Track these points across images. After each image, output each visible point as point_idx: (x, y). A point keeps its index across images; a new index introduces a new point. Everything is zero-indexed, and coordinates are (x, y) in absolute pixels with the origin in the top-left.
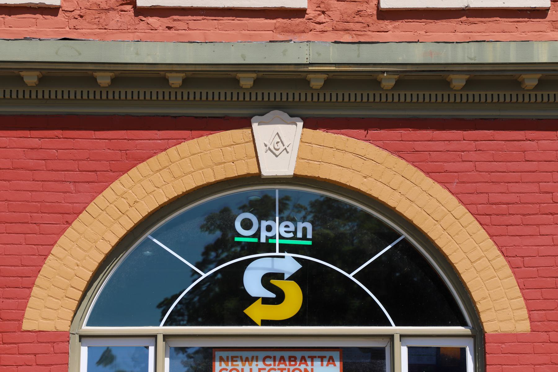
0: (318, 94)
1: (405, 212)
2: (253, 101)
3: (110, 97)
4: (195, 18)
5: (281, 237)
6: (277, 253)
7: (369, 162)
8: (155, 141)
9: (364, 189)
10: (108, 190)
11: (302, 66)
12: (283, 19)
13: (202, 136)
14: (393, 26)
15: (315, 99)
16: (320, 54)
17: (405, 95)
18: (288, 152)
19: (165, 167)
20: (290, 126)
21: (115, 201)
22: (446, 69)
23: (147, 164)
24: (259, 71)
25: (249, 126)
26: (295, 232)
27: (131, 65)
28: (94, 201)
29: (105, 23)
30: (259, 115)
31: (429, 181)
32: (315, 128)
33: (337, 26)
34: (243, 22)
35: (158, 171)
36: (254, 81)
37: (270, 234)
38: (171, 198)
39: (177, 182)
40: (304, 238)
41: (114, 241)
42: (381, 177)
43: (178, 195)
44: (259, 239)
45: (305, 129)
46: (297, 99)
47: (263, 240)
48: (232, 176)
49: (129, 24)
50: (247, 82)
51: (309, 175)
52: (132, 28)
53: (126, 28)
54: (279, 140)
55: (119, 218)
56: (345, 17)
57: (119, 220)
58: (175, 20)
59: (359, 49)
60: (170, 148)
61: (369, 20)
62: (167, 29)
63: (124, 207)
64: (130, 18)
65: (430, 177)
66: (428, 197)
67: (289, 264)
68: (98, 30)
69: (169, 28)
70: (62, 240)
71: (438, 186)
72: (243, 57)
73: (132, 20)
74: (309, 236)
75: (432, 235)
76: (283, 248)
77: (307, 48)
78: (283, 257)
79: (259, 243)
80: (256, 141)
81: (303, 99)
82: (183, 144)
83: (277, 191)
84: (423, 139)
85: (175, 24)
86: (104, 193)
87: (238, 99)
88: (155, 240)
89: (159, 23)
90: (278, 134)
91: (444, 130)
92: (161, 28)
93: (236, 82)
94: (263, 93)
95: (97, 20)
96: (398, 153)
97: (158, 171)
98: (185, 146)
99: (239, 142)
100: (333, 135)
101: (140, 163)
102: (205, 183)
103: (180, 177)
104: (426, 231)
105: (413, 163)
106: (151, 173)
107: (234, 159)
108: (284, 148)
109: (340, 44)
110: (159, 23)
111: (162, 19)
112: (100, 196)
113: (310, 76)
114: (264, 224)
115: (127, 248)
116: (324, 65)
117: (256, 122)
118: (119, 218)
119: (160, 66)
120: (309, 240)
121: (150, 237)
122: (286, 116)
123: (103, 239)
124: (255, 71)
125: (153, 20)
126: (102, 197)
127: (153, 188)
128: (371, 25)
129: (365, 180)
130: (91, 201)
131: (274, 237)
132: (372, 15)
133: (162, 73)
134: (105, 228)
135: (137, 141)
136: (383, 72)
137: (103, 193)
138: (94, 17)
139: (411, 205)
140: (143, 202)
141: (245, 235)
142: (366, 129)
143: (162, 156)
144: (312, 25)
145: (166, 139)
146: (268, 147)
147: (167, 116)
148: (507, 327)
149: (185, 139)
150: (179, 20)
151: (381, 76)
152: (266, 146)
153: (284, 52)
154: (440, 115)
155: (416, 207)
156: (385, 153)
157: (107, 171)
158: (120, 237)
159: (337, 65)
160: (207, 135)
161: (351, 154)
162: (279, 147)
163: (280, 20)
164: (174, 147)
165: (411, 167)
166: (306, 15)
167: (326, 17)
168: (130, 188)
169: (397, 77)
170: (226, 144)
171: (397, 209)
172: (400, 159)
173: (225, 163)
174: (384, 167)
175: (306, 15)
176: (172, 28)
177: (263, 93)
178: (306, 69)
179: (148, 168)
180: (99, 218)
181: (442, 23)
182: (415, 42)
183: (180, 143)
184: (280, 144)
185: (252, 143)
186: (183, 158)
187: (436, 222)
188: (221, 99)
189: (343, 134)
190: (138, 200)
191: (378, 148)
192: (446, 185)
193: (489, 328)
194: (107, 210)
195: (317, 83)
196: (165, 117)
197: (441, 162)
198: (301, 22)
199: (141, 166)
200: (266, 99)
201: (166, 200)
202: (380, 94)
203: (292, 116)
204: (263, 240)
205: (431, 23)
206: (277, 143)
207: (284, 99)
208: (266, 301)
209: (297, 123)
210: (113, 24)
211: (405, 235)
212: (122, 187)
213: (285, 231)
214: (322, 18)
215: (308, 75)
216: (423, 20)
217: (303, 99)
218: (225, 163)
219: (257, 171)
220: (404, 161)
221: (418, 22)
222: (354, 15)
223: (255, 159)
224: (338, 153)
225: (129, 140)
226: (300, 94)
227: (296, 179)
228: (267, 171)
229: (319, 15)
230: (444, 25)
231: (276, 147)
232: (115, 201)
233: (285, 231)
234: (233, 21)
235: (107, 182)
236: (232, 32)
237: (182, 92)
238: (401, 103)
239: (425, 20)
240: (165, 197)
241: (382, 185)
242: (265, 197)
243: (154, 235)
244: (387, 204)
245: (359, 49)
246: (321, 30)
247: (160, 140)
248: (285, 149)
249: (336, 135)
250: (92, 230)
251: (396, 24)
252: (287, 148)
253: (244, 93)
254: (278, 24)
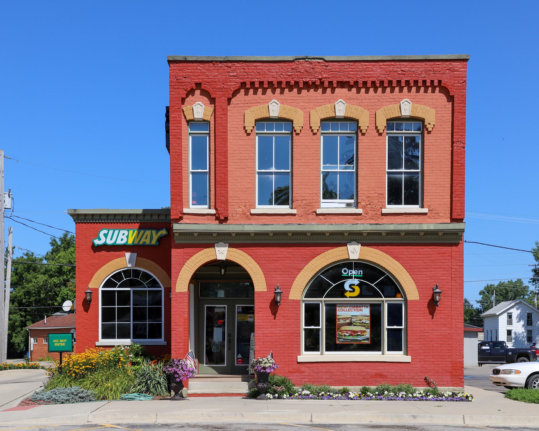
67: (356, 282)
70: (298, 276)
76: (355, 277)
98: (329, 251)
114: (350, 271)
125: (321, 217)
141: (345, 274)
148: (413, 299)
188: (340, 239)
193: (408, 299)
208: (350, 291)
214: (366, 216)
228: (351, 258)
242: (349, 264)
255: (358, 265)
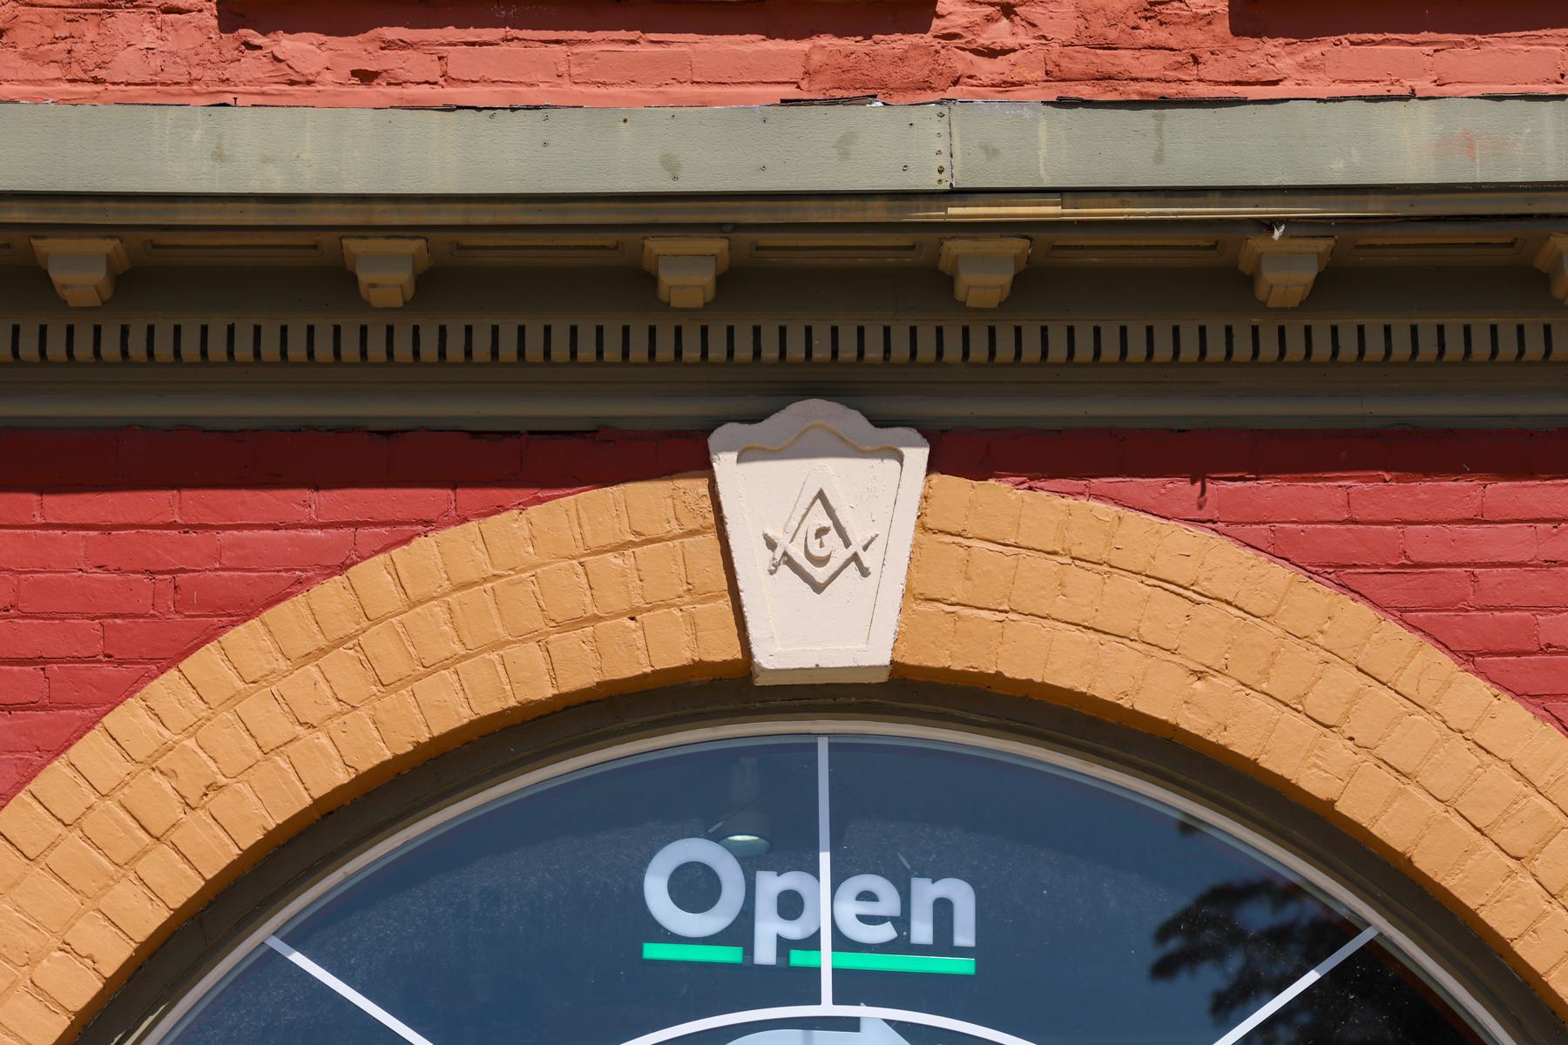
0: (992, 331)
1: (1375, 819)
2: (715, 365)
3: (111, 349)
4: (472, 34)
5: (841, 942)
6: (827, 1007)
7: (1210, 613)
8: (301, 532)
9: (1192, 722)
10: (94, 740)
11: (921, 203)
12: (840, 35)
13: (500, 509)
14: (1300, 59)
15: (979, 352)
16: (996, 151)
17: (1361, 329)
18: (865, 572)
19: (341, 642)
20: (876, 462)
21: (123, 784)
22: (1536, 209)
23: (262, 630)
24: (738, 227)
25: (703, 466)
26: (902, 922)
27: (191, 205)
28: (30, 787)
29: (96, 58)
30: (742, 421)
31: (1471, 693)
32: (977, 469)
33: (1064, 63)
34: (673, 48)
35: (309, 657)
36: (720, 281)
37: (793, 930)
38: (364, 767)
39: (391, 700)
40: (943, 943)
41: (115, 954)
42: (1265, 675)
43: (396, 758)
44: (749, 950)
45: (936, 478)
46: (900, 350)
47: (765, 954)
48: (627, 673)
49: (195, 60)
50: (687, 276)
51: (957, 666)
52: (209, 75)
53: (185, 79)
54: (828, 523)
55: (136, 858)
56: (1098, 27)
57: (139, 866)
58: (388, 45)
59: (1159, 130)
60: (363, 558)
61: (1195, 36)
62: (355, 80)
63: (162, 808)
64: (199, 38)
65: (1479, 673)
66: (1473, 759)
68: (67, 86)
69: (366, 77)
71: (1515, 712)
72: (674, 171)
73: (208, 46)
74: (964, 936)
75: (1501, 919)
76: (851, 986)
77: (940, 126)
78: (852, 1024)
79: (748, 967)
80: (729, 528)
81: (926, 351)
82: (417, 542)
83: (823, 745)
84: (1441, 516)
85: (390, 61)
86: (77, 752)
87: (652, 353)
88: (298, 958)
89: (323, 58)
90: (821, 495)
91: (1531, 475)
92: (328, 76)
93: (640, 282)
94: (757, 331)
95: (62, 46)
96: (1337, 571)
97: (309, 657)
98: (426, 548)
99: (660, 532)
100: (1057, 500)
101: (233, 624)
102: (512, 703)
103: (403, 681)
104: (1471, 902)
105: (1402, 613)
106: (283, 665)
107: (638, 601)
108: (848, 553)
109: (1081, 111)
110: (323, 58)
111: (334, 41)
112: (59, 764)
113: (956, 246)
114: (770, 885)
115: (171, 994)
116: (1013, 198)
117: (729, 450)
118: (136, 858)
119: (315, 206)
120: (962, 952)
121: (277, 944)
122: (854, 422)
123: (66, 947)
124: (718, 227)
126: (69, 771)
127: (288, 729)
128: (1206, 56)
129: (1199, 685)
130: (19, 787)
131: (812, 942)
132: (1209, 19)
133: (325, 238)
134: (76, 899)
135: (223, 535)
136: (1269, 225)
137: (72, 751)
138: (48, 33)
139: (1401, 792)
140: (244, 788)
141: (686, 931)
142: (1198, 474)
143: (329, 594)
144: (962, 61)
145: (348, 524)
146: (779, 553)
147: (353, 430)
149: (427, 523)
150: (406, 45)
151: (1256, 243)
152: (771, 545)
153: (844, 146)
154: (1514, 417)
155: (1425, 797)
156: (1280, 574)
157: (92, 659)
158: (141, 938)
159: (1068, 198)
160: (523, 505)
161: (1134, 581)
162: (827, 549)
163: (826, 41)
164: (381, 558)
165: (1392, 628)
166: (935, 22)
167: (1019, 30)
168: (190, 730)
169: (1323, 245)
170: (603, 541)
171: (1341, 807)
172: (1345, 599)
173: (599, 619)
174: (1277, 631)
175: (935, 22)
176: (376, 75)
177: (757, 331)
178: (935, 215)
179: (267, 643)
180: (52, 858)
181: (1505, 47)
182: (1400, 98)
183: (407, 541)
184: (832, 537)
185: (712, 538)
186: (420, 603)
187: (1512, 863)
189: (1098, 497)
190: (222, 780)
191: (1249, 552)
192: (1548, 704)
194: (85, 823)
195: (984, 279)
196: (342, 431)
197: (1527, 609)
198: (915, 47)
199: (237, 636)
200: (770, 352)
201: (343, 777)
202: (1255, 329)
203: (879, 422)
204: (765, 954)
205: (1461, 44)
206: (821, 532)
207: (848, 352)
209: (906, 451)
210: (127, 64)
211: (1378, 925)
212: (153, 724)
213: (864, 919)
214: (1001, 32)
215: (948, 244)
216: (1425, 36)
217: (926, 351)
218: (599, 619)
219: (735, 653)
220: (1363, 608)
221: (1402, 42)
222: (1133, 20)
223: (725, 604)
224: (1081, 578)
225: (186, 528)
226: (913, 330)
227: (905, 690)
229: (989, 19)
230: (1513, 52)
231: (816, 551)
232: (123, 784)
233: (864, 919)
234: (632, 48)
235: (88, 706)
236: (626, 89)
237: (416, 329)
238: (1345, 364)
239: (1434, 36)
240: (338, 764)
241: (1271, 708)
243: (296, 939)
244: (1297, 788)
245: (1159, 130)
246: (998, 79)
247: (322, 526)
248: (855, 558)
249: (1069, 500)
250: (19, 909)
251: (1313, 50)
252: (863, 556)
253: (678, 331)
254: (817, 58)
255: (936, 750)
